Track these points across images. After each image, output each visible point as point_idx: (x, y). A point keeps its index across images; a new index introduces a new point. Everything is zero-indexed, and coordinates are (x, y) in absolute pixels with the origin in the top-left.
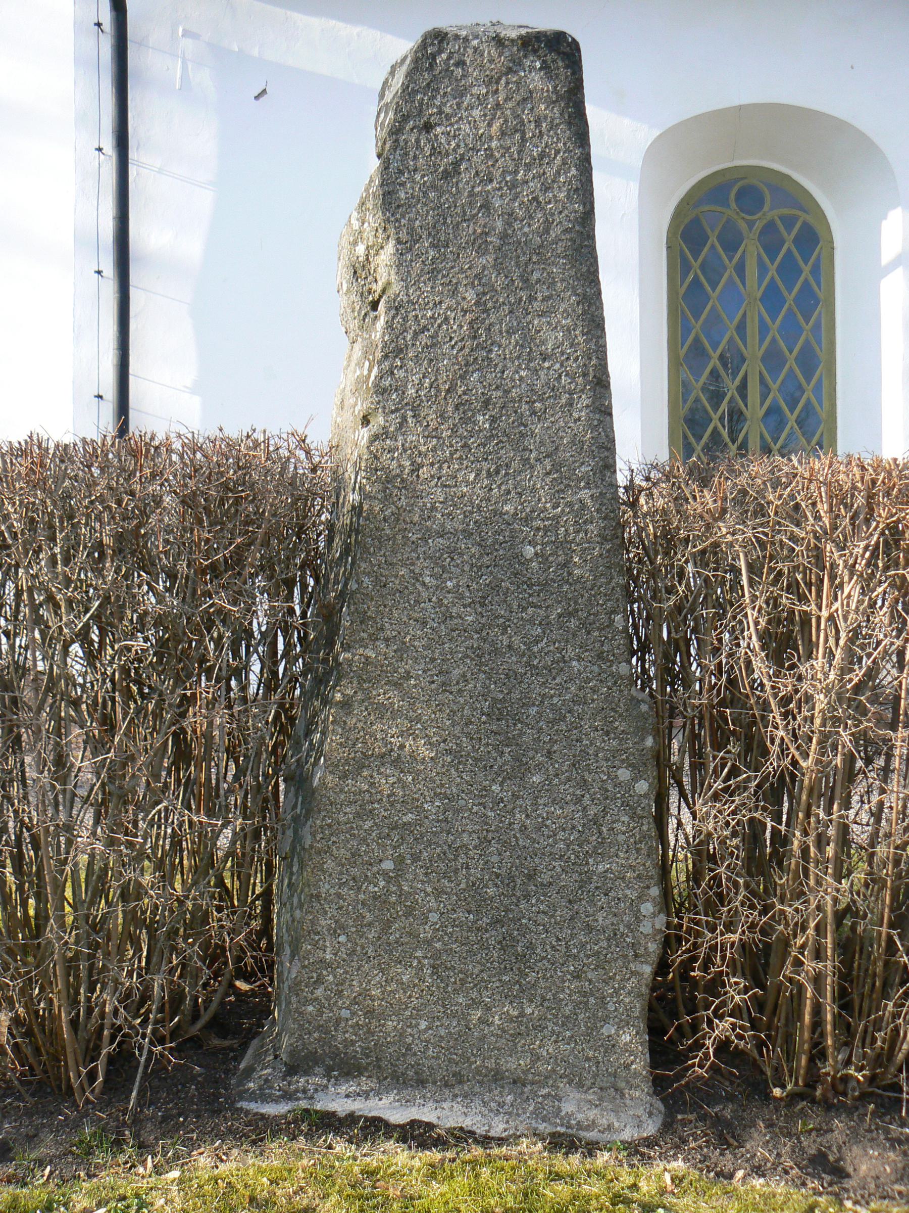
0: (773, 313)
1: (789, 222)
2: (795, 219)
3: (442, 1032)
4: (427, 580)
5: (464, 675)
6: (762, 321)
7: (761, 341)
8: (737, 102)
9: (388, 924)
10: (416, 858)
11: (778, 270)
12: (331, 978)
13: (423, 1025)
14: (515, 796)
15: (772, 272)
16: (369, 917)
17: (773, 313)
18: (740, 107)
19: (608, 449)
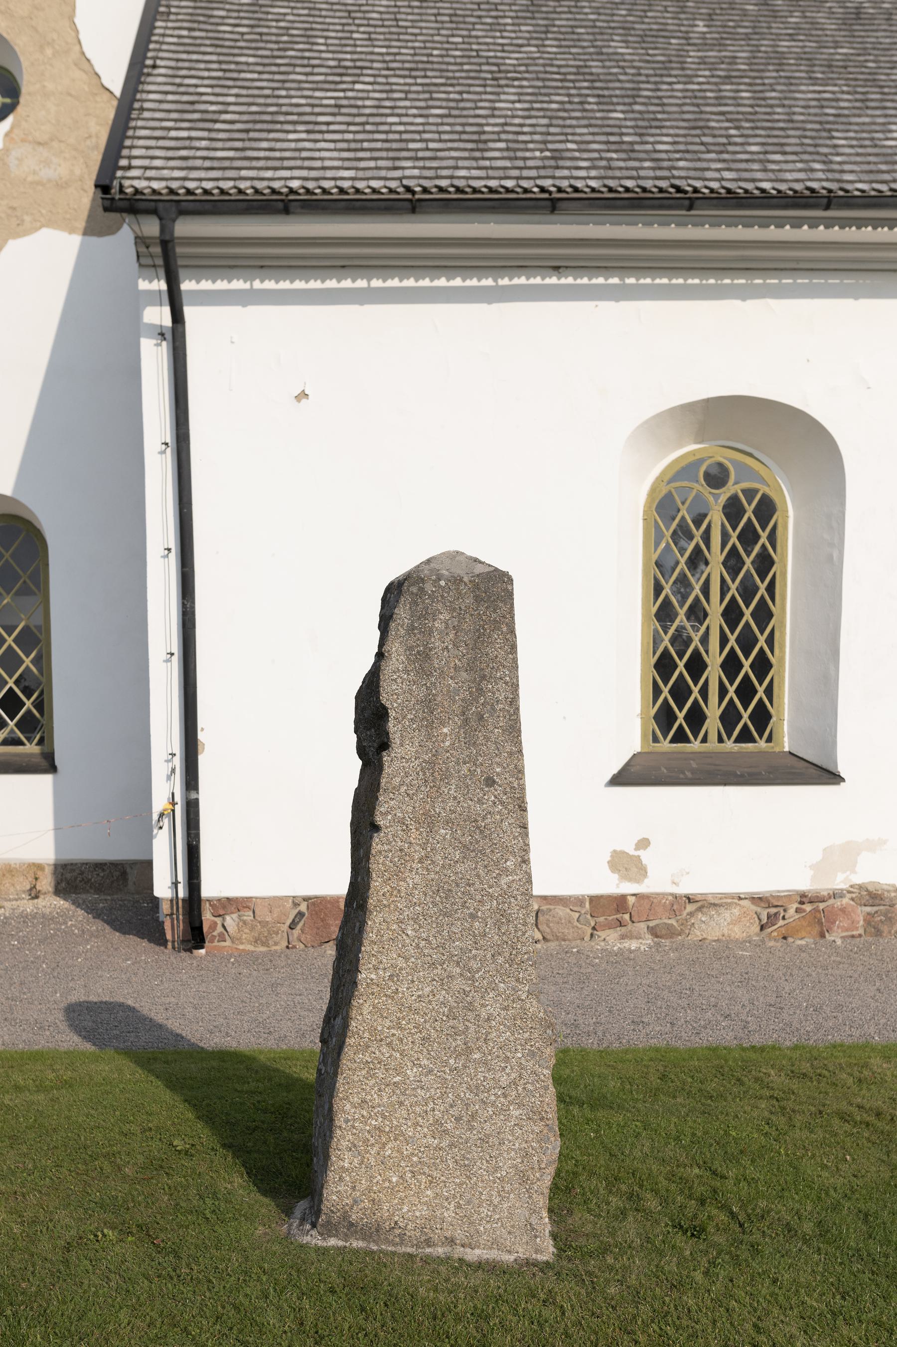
0: (696, 655)
1: (750, 494)
2: (756, 491)
3: (418, 1214)
4: (409, 932)
5: (432, 991)
6: (723, 580)
7: (722, 600)
8: (705, 397)
9: (384, 1145)
10: (401, 1104)
11: (739, 538)
12: (348, 1178)
13: (405, 1209)
14: (465, 1067)
15: (734, 540)
16: (372, 1141)
17: (696, 655)
18: (708, 400)
19: (525, 850)
